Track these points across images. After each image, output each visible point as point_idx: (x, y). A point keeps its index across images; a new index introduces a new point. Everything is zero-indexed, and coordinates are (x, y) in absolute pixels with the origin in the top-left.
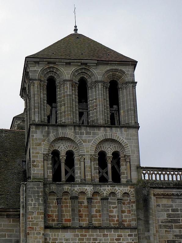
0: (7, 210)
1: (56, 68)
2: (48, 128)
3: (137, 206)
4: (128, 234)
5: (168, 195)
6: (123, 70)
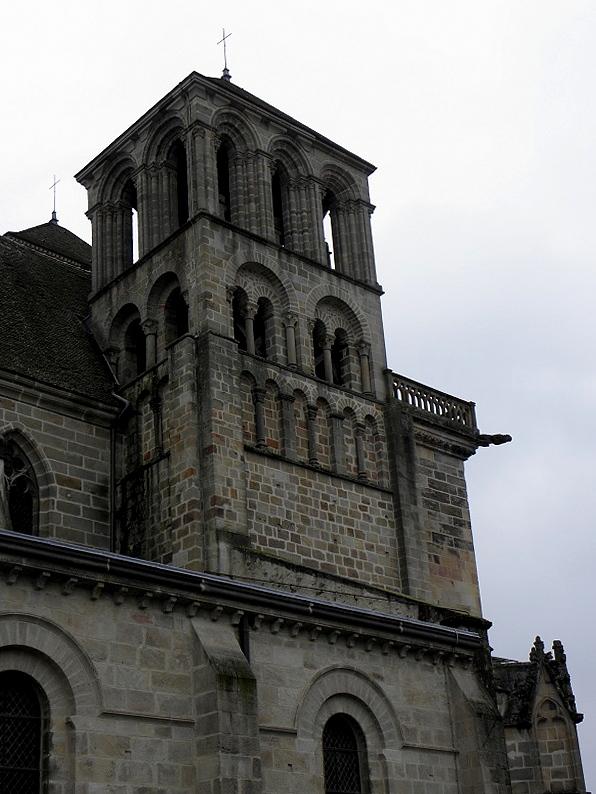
0: (93, 403)
1: (242, 121)
2: (234, 236)
4: (378, 501)
5: (432, 442)
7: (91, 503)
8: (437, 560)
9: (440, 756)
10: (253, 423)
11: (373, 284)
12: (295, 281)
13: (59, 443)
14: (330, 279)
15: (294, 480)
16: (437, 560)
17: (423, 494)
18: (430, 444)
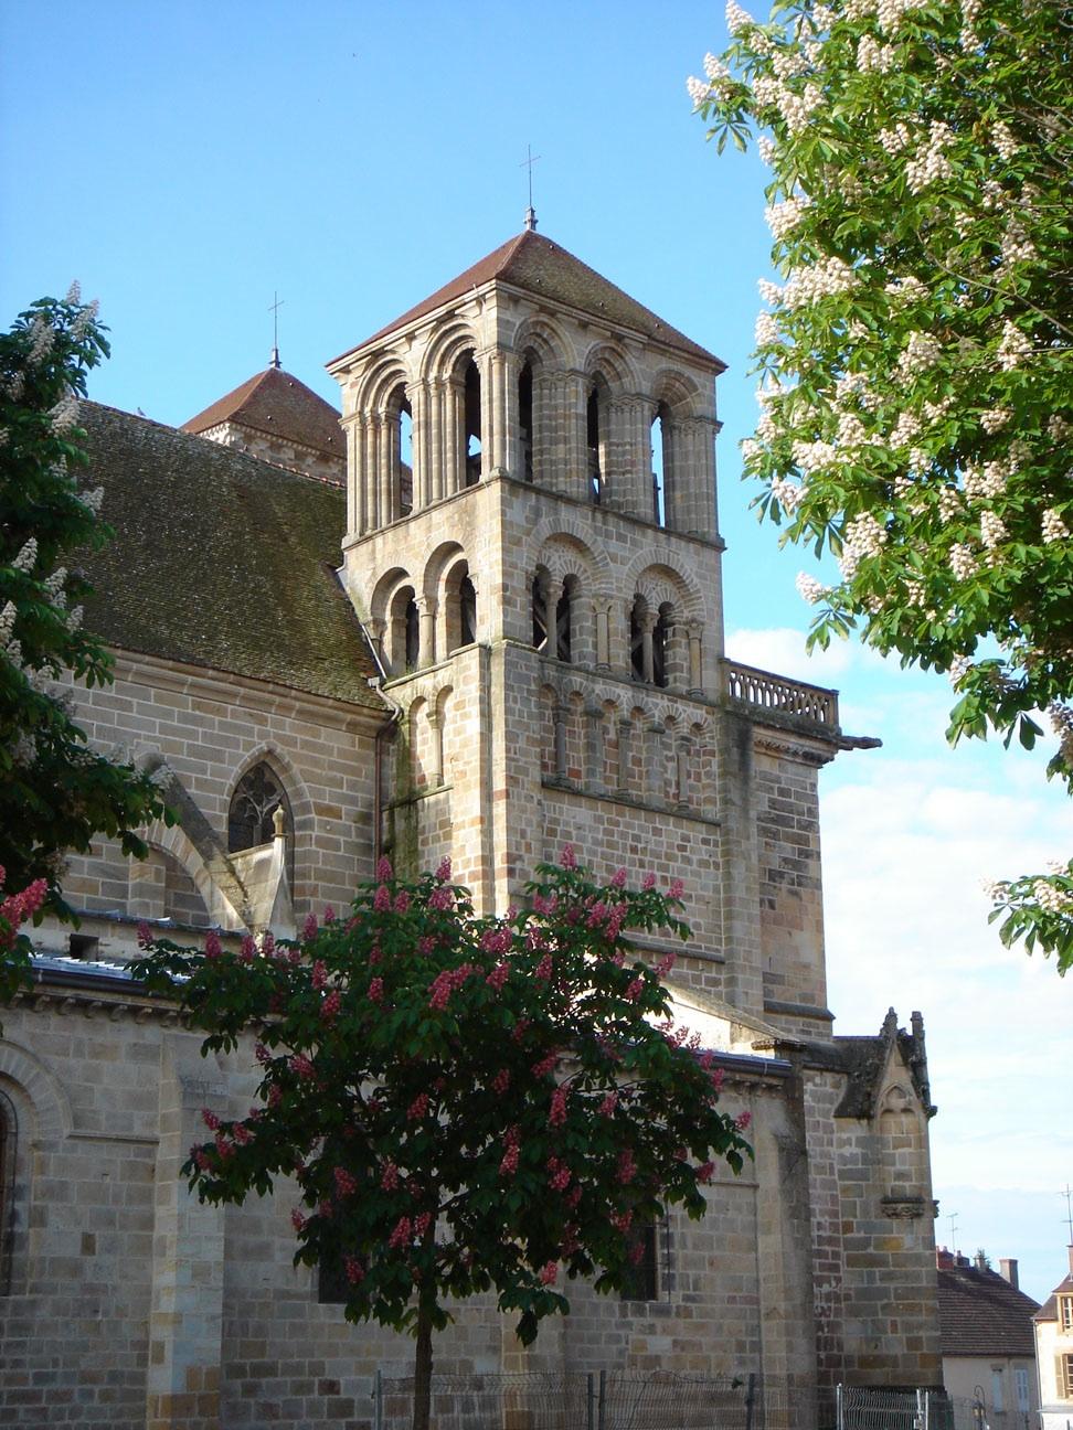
1: (552, 329)
2: (538, 500)
3: (723, 764)
5: (777, 749)
6: (695, 380)
7: (353, 833)
8: (772, 906)
9: (738, 1190)
10: (552, 749)
11: (712, 538)
12: (612, 550)
13: (316, 762)
14: (656, 540)
15: (599, 820)
16: (772, 906)
17: (759, 819)
18: (773, 750)
